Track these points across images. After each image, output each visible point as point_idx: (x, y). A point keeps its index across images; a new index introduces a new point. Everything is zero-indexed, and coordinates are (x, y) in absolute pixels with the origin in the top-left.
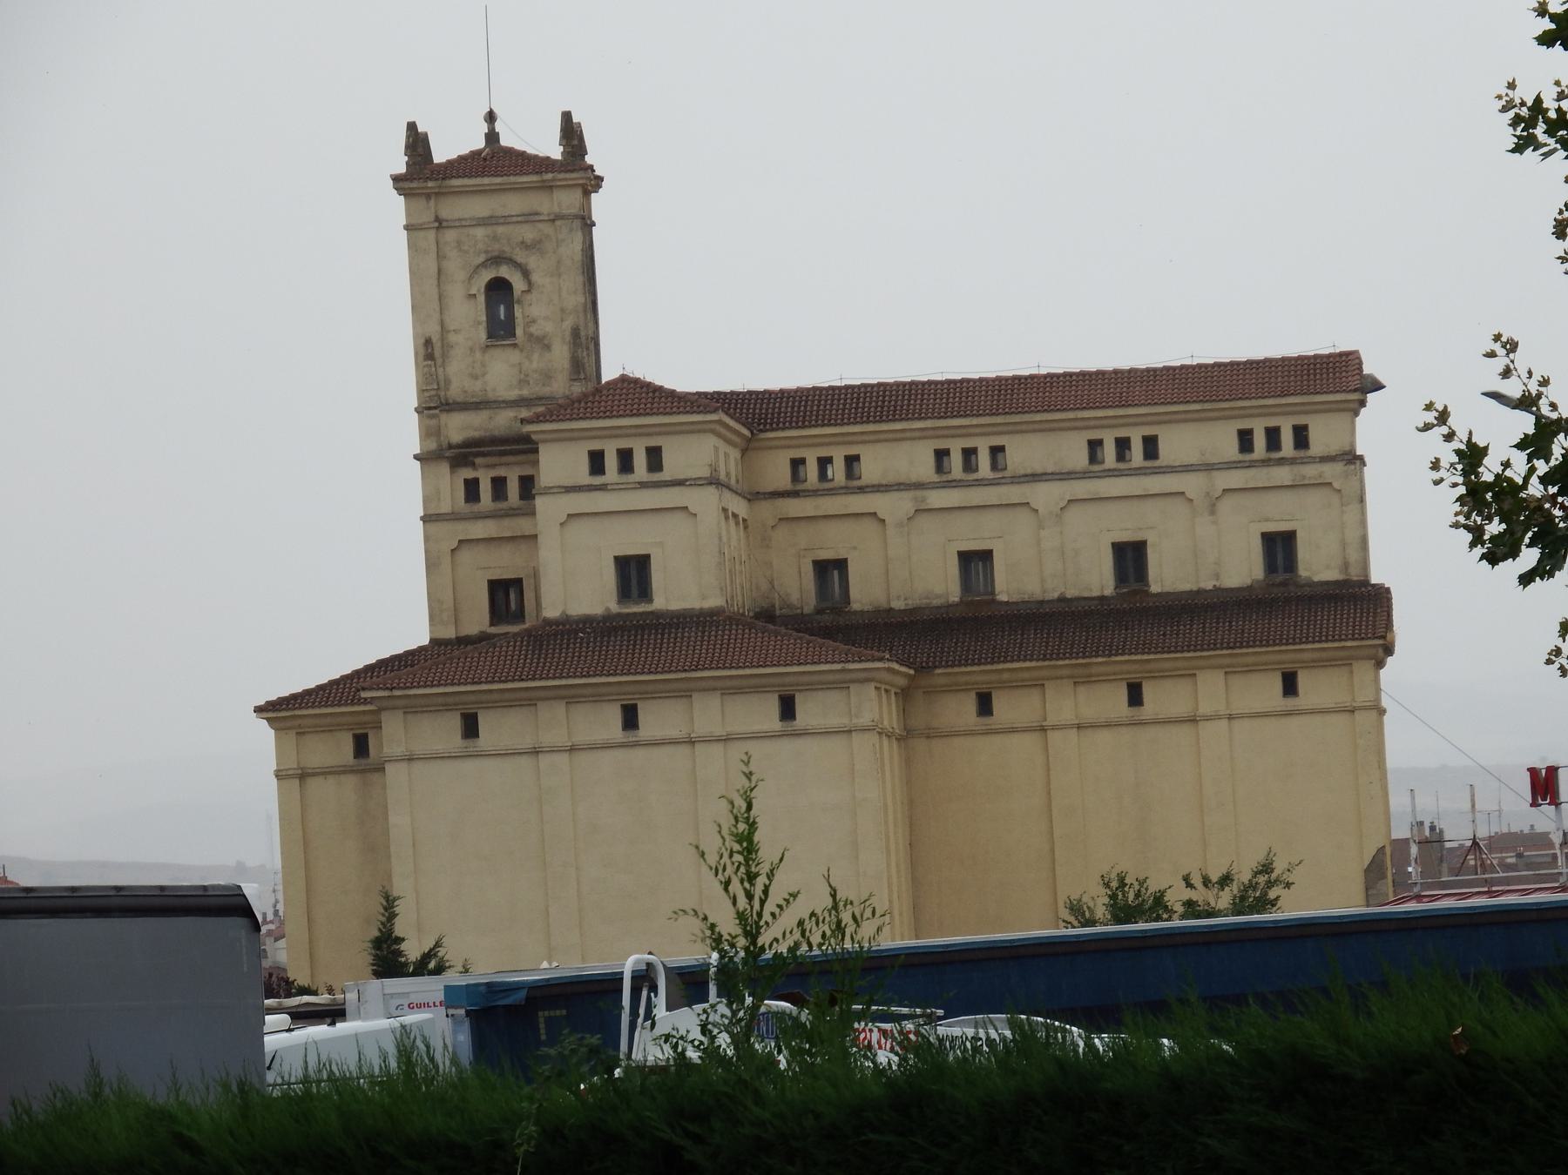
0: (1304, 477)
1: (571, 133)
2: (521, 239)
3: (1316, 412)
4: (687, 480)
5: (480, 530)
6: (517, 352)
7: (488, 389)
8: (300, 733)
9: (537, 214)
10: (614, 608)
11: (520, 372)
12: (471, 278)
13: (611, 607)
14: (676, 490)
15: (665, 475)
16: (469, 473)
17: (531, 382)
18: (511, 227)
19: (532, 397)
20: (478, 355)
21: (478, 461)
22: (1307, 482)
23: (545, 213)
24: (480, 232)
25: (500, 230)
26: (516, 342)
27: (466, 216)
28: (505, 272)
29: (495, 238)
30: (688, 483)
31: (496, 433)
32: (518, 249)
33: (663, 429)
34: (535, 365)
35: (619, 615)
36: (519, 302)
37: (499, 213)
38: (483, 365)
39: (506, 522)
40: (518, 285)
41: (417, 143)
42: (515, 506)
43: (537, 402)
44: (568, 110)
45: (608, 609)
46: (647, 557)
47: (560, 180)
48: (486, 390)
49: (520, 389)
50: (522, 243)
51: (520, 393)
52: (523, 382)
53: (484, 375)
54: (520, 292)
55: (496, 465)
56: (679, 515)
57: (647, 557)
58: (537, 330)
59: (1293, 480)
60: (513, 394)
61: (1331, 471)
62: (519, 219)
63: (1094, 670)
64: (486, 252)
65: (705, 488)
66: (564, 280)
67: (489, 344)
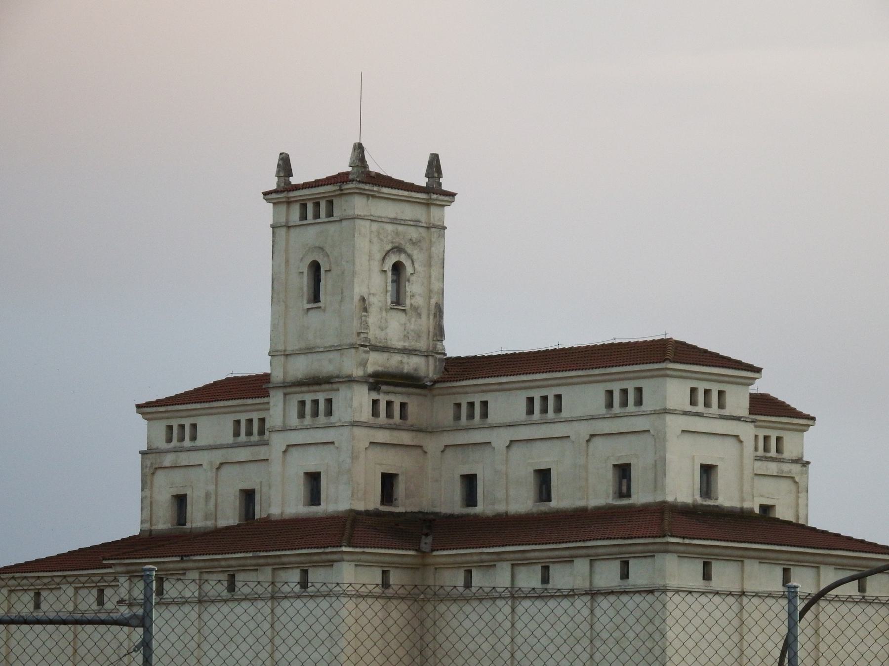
0: (782, 472)
1: (434, 166)
2: (410, 237)
3: (790, 430)
4: (742, 417)
5: (382, 436)
6: (404, 314)
7: (388, 338)
8: (357, 565)
9: (419, 221)
10: (699, 500)
11: (405, 330)
12: (384, 259)
13: (698, 500)
14: (735, 423)
15: (726, 412)
16: (375, 396)
17: (410, 338)
18: (406, 227)
19: (410, 348)
20: (384, 313)
21: (384, 388)
22: (784, 475)
23: (424, 221)
24: (390, 227)
25: (401, 228)
26: (406, 308)
27: (383, 215)
28: (403, 258)
29: (397, 234)
30: (742, 419)
31: (390, 370)
32: (408, 243)
33: (732, 379)
34: (412, 327)
35: (702, 505)
36: (409, 281)
37: (399, 217)
38: (386, 321)
39: (396, 433)
40: (409, 269)
41: (285, 166)
42: (397, 423)
43: (413, 352)
44: (437, 153)
45: (695, 500)
46: (549, 470)
47: (440, 200)
48: (387, 339)
49: (404, 342)
50: (411, 240)
51: (404, 344)
52: (406, 337)
53: (386, 328)
54: (409, 274)
55: (389, 393)
56: (733, 441)
57: (549, 470)
58: (414, 302)
59: (778, 472)
60: (400, 345)
61: (796, 468)
62: (412, 223)
63: (619, 588)
64: (392, 242)
65: (749, 424)
66: (433, 270)
67: (392, 307)
